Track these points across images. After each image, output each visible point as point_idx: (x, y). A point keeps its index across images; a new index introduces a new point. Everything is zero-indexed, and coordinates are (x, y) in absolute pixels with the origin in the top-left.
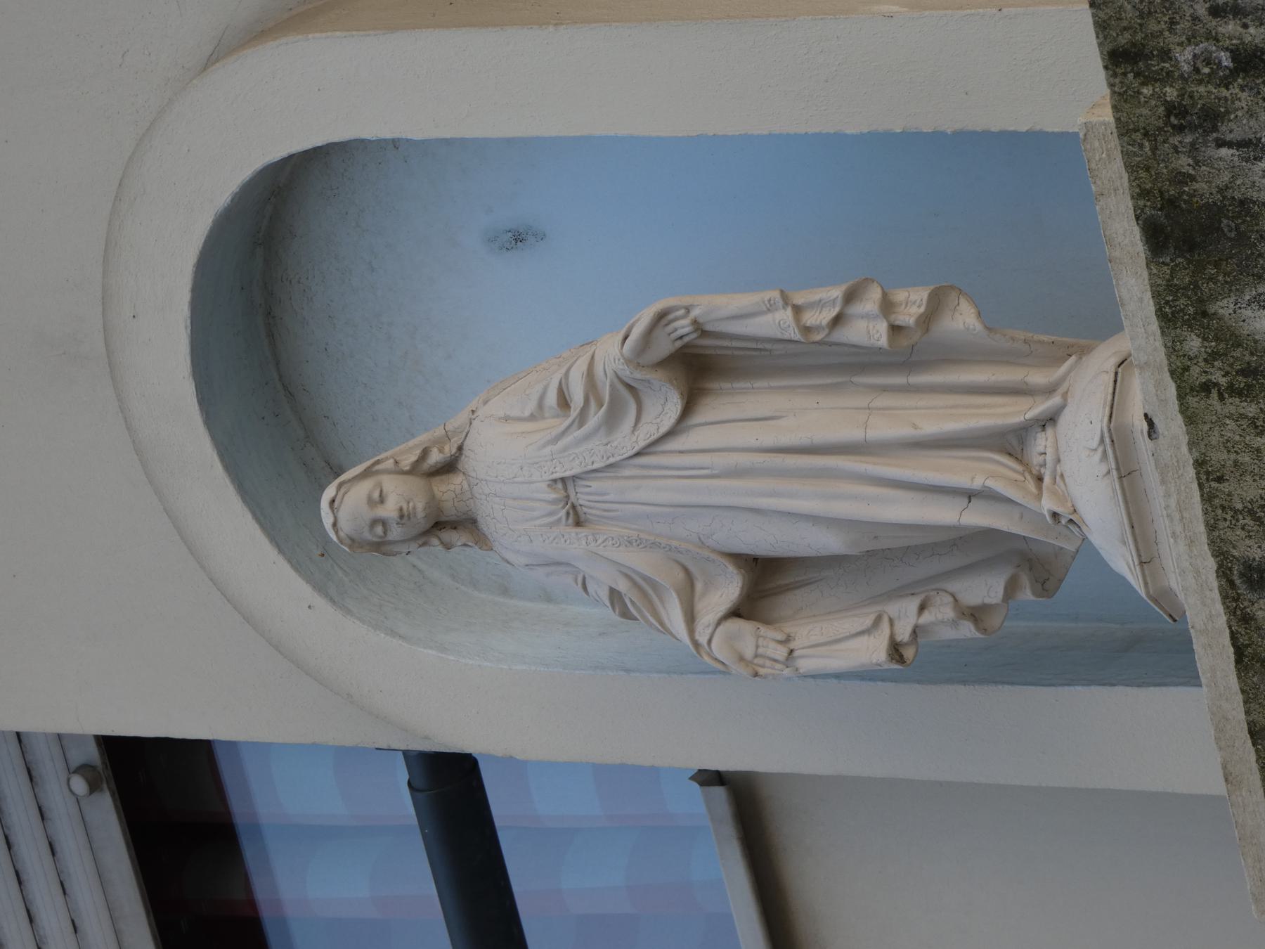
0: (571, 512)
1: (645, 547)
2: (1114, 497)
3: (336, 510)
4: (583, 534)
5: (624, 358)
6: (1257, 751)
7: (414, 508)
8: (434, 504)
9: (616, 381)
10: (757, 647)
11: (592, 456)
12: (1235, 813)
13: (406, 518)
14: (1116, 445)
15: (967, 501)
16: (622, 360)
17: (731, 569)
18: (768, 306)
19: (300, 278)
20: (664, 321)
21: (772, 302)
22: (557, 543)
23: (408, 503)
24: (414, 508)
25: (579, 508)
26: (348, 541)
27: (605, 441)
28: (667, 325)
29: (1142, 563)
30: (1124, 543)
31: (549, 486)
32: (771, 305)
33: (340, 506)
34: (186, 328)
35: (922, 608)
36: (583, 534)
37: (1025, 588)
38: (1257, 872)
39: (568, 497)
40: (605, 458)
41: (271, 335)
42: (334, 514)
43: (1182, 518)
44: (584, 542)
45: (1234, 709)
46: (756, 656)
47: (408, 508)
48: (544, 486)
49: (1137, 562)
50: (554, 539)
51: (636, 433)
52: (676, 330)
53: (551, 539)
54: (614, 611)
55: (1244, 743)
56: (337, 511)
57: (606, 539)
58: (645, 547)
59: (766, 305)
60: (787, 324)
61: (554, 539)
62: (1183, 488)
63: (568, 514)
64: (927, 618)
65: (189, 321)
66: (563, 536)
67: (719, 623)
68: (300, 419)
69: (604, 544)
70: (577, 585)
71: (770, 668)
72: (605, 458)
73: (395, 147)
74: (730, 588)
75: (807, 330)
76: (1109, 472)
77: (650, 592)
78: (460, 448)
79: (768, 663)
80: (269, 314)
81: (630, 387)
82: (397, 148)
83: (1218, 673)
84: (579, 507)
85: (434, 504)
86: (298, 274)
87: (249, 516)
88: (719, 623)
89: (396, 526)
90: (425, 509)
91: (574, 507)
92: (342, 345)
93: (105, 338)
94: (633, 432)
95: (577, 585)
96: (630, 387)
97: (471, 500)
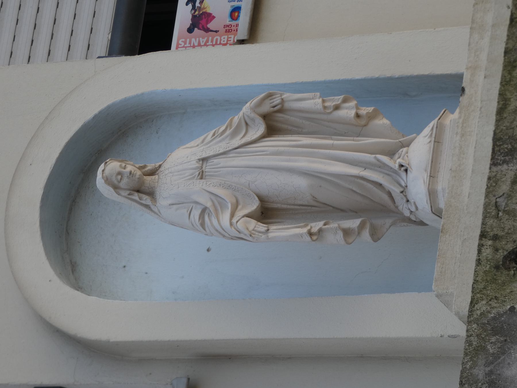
0: (201, 173)
1: (225, 188)
2: (429, 150)
3: (106, 166)
4: (202, 182)
5: (250, 107)
6: (505, 59)
7: (136, 173)
8: (141, 182)
9: (242, 118)
10: (255, 227)
11: (220, 148)
12: (440, 245)
13: (131, 175)
14: (438, 129)
15: (364, 169)
16: (249, 107)
17: (257, 198)
18: (313, 96)
19: (94, 186)
20: (270, 98)
21: (315, 95)
22: (189, 186)
23: (135, 171)
24: (136, 173)
25: (204, 173)
26: (105, 179)
27: (227, 142)
28: (270, 100)
29: (430, 176)
30: (426, 170)
31: (197, 162)
32: (314, 96)
33: (108, 165)
34: (51, 168)
35: (325, 225)
36: (202, 182)
37: (367, 229)
38: (440, 269)
39: (202, 168)
40: (225, 148)
41: (71, 210)
42: (105, 167)
43: (463, 126)
44: (201, 185)
45: (455, 202)
46: (253, 230)
47: (134, 172)
48: (194, 162)
49: (429, 175)
50: (189, 185)
51: (241, 140)
52: (273, 102)
53: (188, 185)
54: (199, 221)
55: (454, 216)
56: (107, 166)
57: (211, 183)
58: (225, 188)
59: (312, 96)
60: (318, 103)
61: (189, 185)
62: (467, 114)
63: (199, 174)
64: (327, 226)
65: (53, 165)
66: (193, 183)
67: (243, 217)
68: (67, 244)
69: (209, 186)
70: (187, 212)
71: (257, 235)
72: (225, 148)
73: (157, 132)
74: (254, 205)
75: (325, 107)
76: (430, 142)
77: (219, 208)
78: (160, 166)
79: (257, 233)
80: (74, 201)
81: (247, 124)
82: (157, 133)
83: (454, 187)
84: (205, 172)
85: (141, 182)
86: (94, 184)
87: (41, 244)
88: (243, 217)
89: (126, 178)
90: (140, 175)
91: (203, 172)
92: (99, 212)
93: (15, 173)
94: (240, 139)
95: (187, 212)
96: (247, 124)
97: (157, 183)
